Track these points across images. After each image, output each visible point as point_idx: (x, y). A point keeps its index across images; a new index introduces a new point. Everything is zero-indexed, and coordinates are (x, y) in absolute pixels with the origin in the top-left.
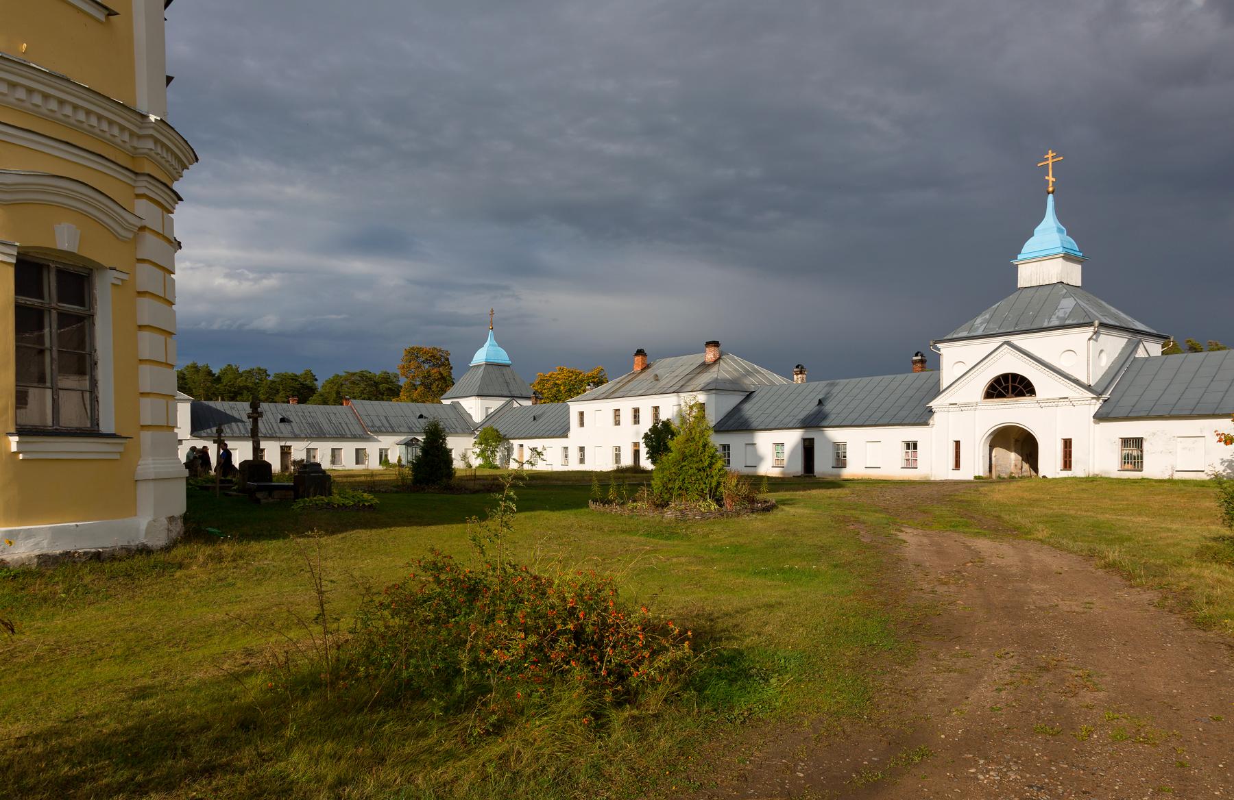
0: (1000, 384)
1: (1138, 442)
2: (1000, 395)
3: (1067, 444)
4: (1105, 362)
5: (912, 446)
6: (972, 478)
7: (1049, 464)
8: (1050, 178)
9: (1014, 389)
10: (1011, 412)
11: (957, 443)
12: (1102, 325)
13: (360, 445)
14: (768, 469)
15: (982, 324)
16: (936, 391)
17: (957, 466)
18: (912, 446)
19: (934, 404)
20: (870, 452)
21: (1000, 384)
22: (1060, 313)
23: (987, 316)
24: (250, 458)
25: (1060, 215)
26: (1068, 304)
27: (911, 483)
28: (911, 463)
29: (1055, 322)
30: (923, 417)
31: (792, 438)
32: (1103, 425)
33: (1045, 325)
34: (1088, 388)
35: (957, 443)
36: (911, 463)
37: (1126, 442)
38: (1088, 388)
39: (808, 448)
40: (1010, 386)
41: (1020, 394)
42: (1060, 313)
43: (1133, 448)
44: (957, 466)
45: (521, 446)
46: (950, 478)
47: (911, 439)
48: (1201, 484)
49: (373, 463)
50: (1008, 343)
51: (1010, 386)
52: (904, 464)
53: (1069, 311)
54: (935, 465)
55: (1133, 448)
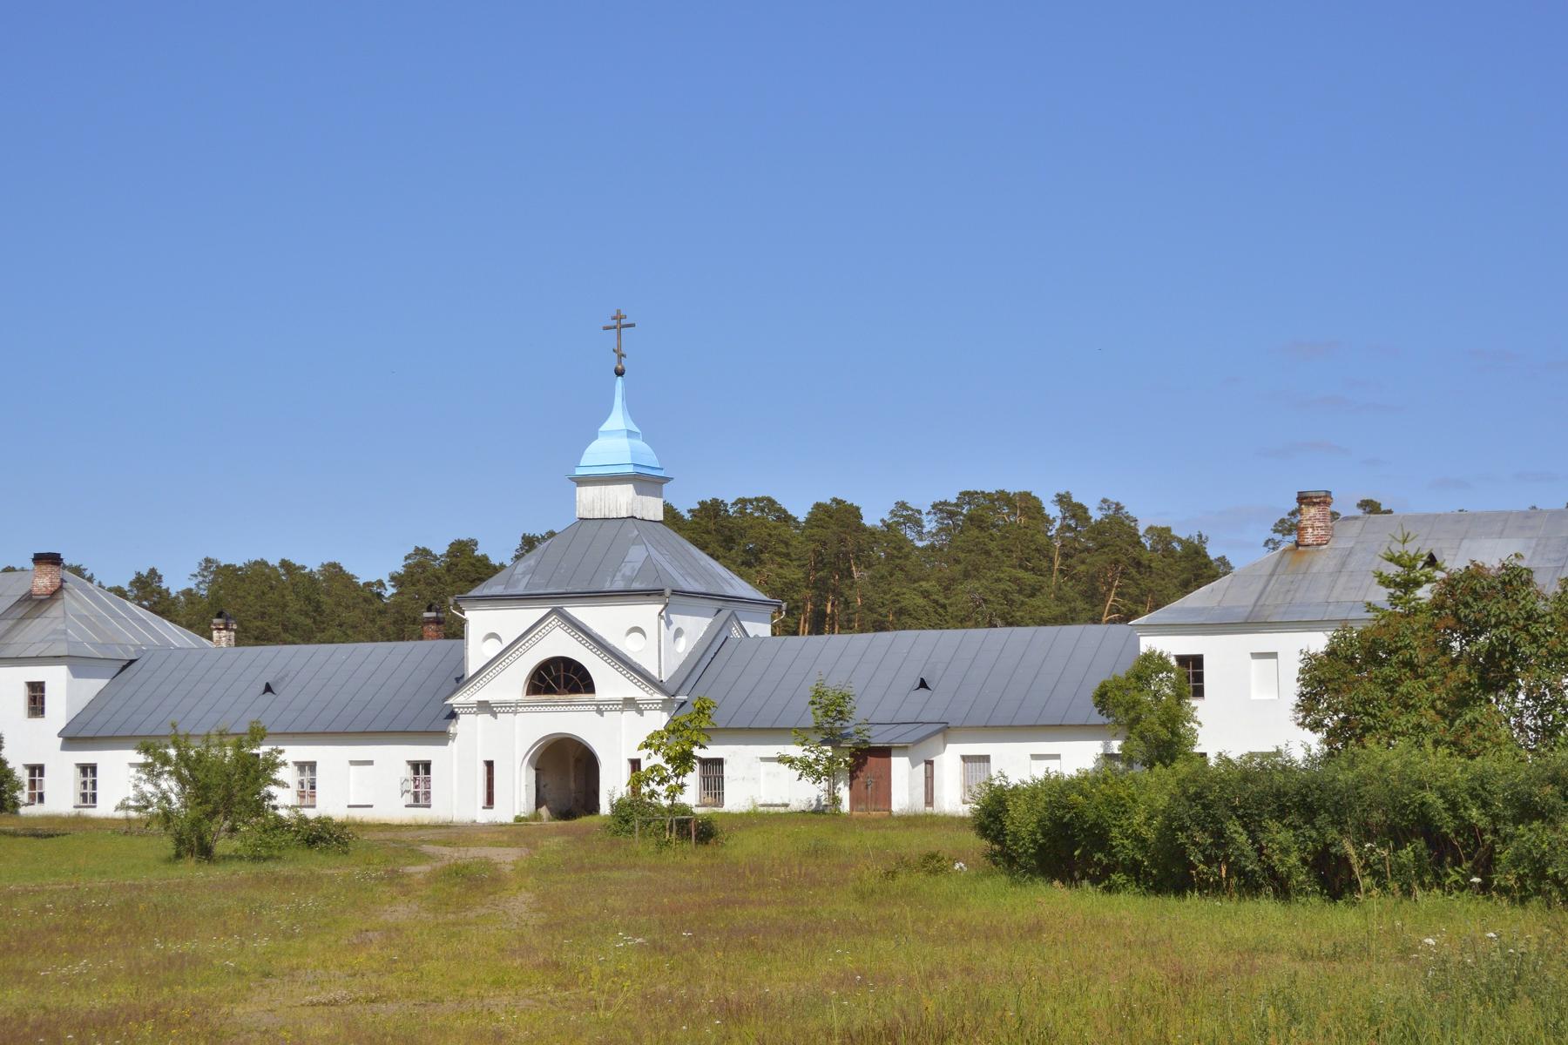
0: (549, 673)
3: (370, 763)
4: (683, 647)
5: (421, 768)
6: (510, 820)
9: (568, 680)
11: (490, 765)
12: (674, 592)
13: (420, 752)
15: (524, 574)
16: (460, 681)
17: (490, 801)
19: (457, 700)
20: (351, 783)
21: (549, 673)
22: (627, 570)
23: (532, 562)
24: (631, 486)
25: (633, 410)
28: (420, 798)
33: (607, 587)
34: (657, 685)
35: (490, 765)
37: (415, 766)
38: (657, 685)
40: (561, 678)
41: (575, 690)
42: (627, 570)
44: (490, 801)
45: (308, 767)
50: (554, 611)
51: (561, 678)
52: (409, 799)
53: (638, 566)
54: (457, 799)
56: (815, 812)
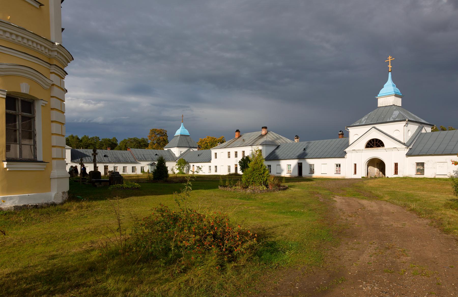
0: (371, 143)
1: (422, 164)
2: (371, 147)
3: (396, 165)
4: (410, 134)
5: (338, 166)
6: (361, 178)
7: (389, 172)
8: (390, 66)
9: (376, 144)
10: (375, 153)
11: (355, 165)
12: (409, 121)
13: (134, 165)
14: (285, 174)
15: (364, 120)
16: (347, 145)
17: (355, 173)
18: (338, 166)
19: (346, 150)
20: (323, 168)
21: (371, 143)
22: (394, 116)
23: (366, 117)
25: (394, 80)
26: (396, 113)
27: (338, 179)
28: (338, 172)
29: (392, 120)
30: (343, 155)
31: (294, 163)
32: (409, 158)
33: (388, 121)
34: (404, 144)
35: (355, 165)
36: (338, 172)
37: (418, 164)
38: (404, 144)
39: (300, 166)
40: (375, 143)
41: (379, 146)
42: (394, 116)
43: (421, 167)
44: (355, 173)
45: (194, 165)
46: (353, 177)
47: (338, 163)
48: (446, 180)
49: (138, 172)
50: (374, 127)
51: (375, 143)
52: (335, 172)
53: (397, 115)
54: (347, 173)
55: (421, 167)
56: (213, 144)
